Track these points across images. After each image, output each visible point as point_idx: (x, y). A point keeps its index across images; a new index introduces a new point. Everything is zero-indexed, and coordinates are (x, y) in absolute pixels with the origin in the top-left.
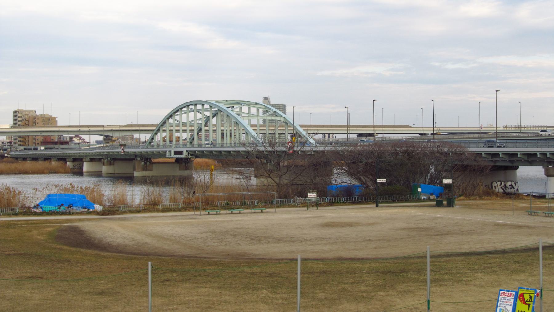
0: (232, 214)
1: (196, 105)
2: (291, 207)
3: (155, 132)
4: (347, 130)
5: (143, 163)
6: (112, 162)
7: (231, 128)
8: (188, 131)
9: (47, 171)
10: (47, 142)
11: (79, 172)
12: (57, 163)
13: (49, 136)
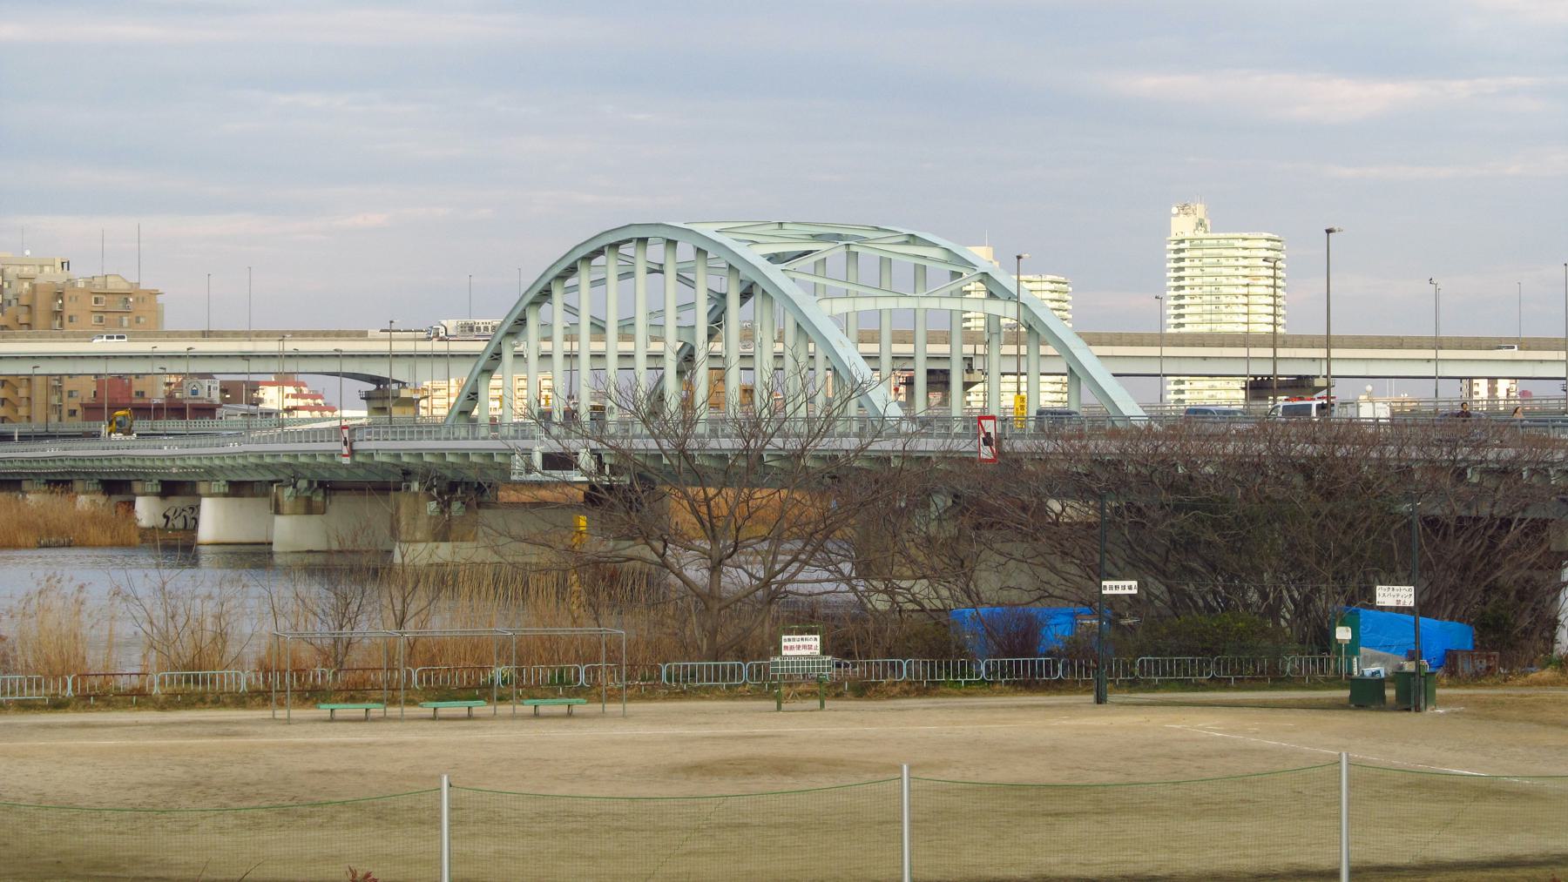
0: (434, 718)
1: (643, 241)
2: (743, 697)
3: (481, 364)
4: (1275, 359)
5: (433, 505)
6: (318, 498)
7: (779, 347)
8: (558, 359)
9: (32, 540)
10: (118, 403)
11: (179, 544)
12: (101, 499)
13: (120, 376)
